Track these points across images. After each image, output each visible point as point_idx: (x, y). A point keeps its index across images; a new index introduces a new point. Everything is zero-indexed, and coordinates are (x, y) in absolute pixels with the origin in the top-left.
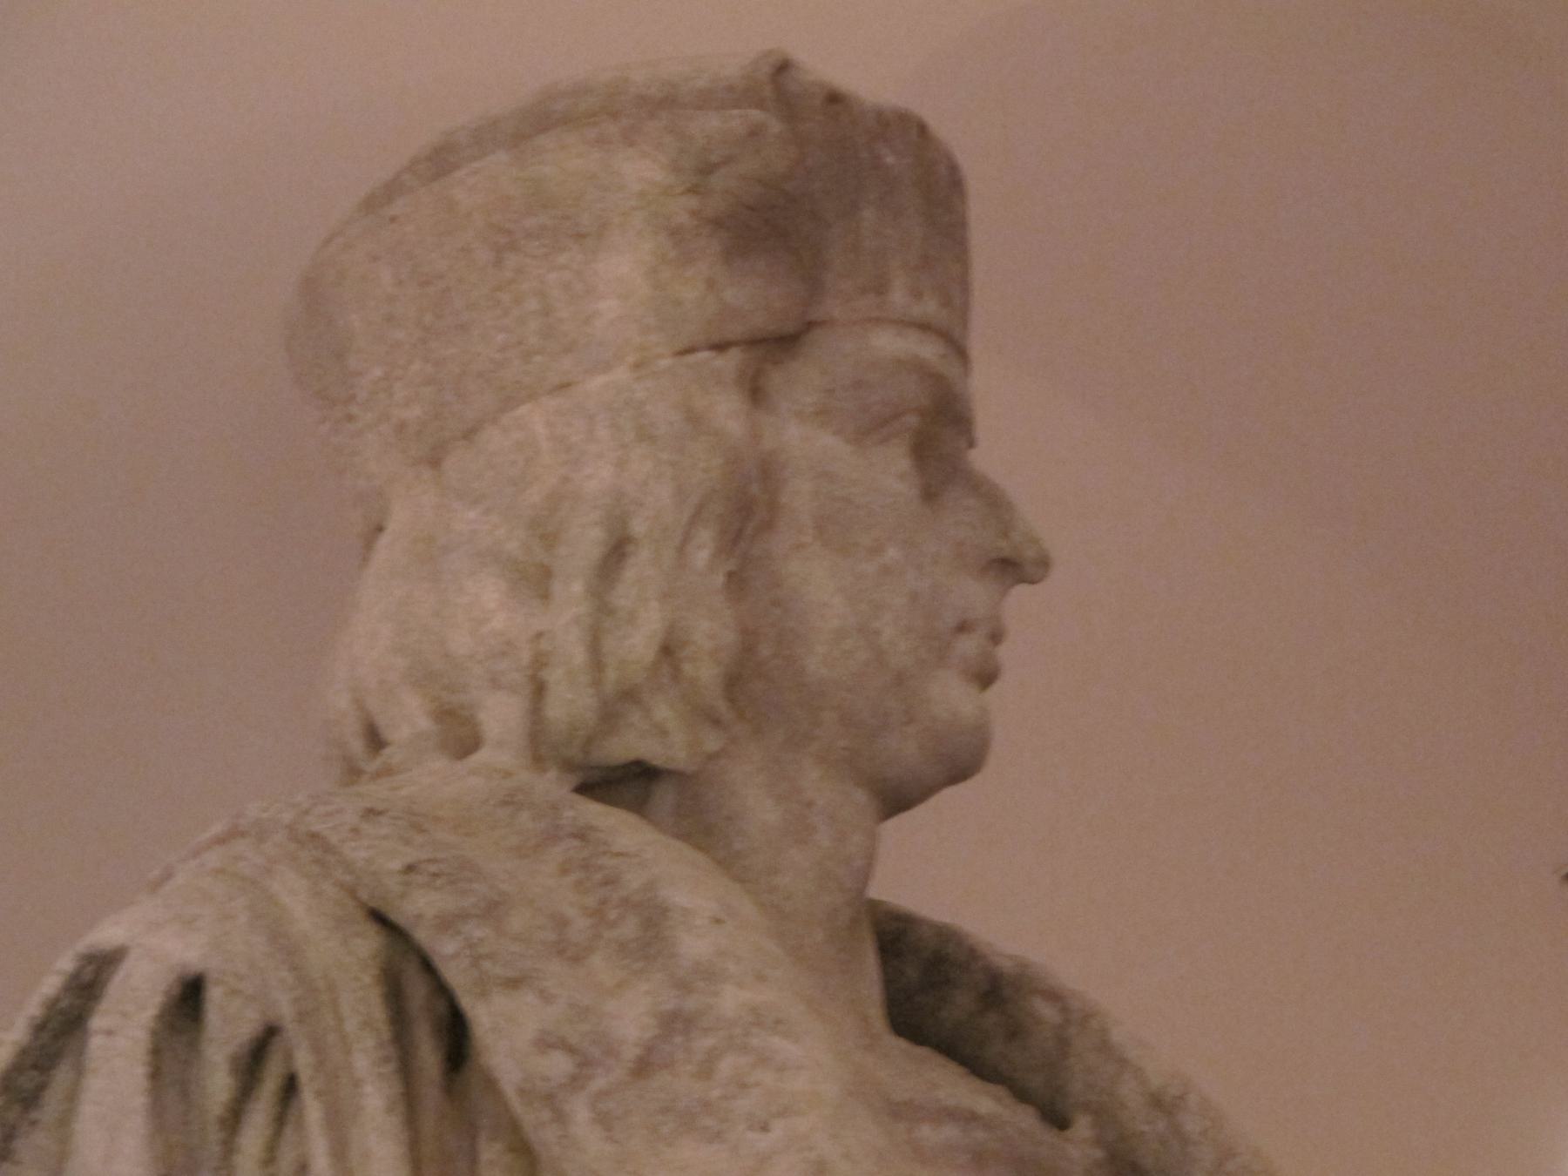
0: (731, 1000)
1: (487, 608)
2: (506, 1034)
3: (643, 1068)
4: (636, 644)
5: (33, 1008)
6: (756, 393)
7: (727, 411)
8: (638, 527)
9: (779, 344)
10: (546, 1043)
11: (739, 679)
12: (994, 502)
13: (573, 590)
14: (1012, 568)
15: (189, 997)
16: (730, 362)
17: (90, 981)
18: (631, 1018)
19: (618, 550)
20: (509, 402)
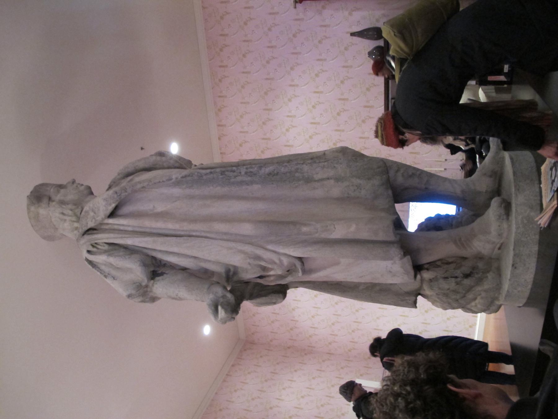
0: (91, 205)
1: (67, 225)
2: (91, 225)
3: (95, 213)
4: (70, 212)
5: (88, 265)
6: (53, 201)
7: (54, 203)
8: (61, 211)
9: (50, 199)
10: (92, 221)
11: (75, 205)
12: (69, 183)
13: (65, 217)
14: (74, 182)
15: (89, 252)
16: (51, 203)
17: (87, 260)
18: (92, 214)
19: (63, 214)
20: (51, 222)
